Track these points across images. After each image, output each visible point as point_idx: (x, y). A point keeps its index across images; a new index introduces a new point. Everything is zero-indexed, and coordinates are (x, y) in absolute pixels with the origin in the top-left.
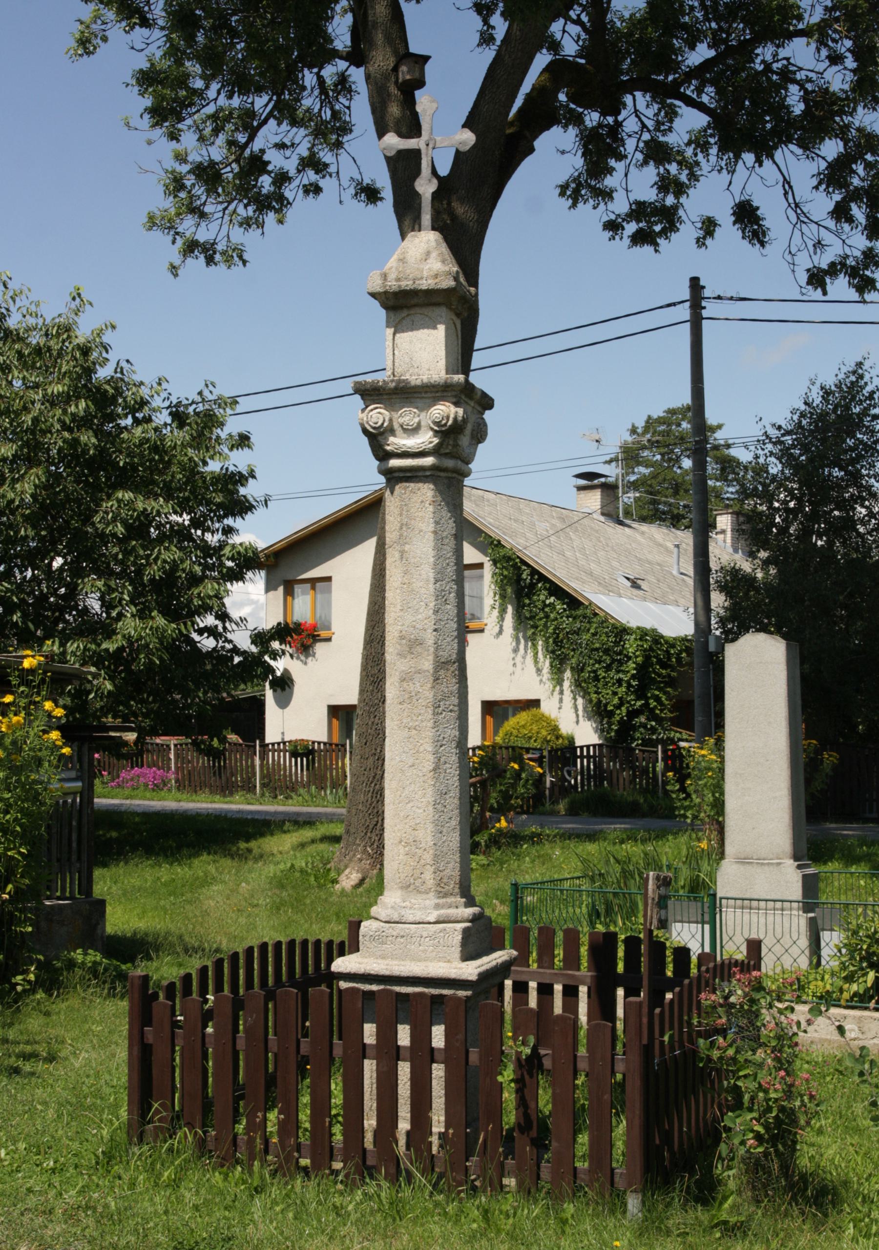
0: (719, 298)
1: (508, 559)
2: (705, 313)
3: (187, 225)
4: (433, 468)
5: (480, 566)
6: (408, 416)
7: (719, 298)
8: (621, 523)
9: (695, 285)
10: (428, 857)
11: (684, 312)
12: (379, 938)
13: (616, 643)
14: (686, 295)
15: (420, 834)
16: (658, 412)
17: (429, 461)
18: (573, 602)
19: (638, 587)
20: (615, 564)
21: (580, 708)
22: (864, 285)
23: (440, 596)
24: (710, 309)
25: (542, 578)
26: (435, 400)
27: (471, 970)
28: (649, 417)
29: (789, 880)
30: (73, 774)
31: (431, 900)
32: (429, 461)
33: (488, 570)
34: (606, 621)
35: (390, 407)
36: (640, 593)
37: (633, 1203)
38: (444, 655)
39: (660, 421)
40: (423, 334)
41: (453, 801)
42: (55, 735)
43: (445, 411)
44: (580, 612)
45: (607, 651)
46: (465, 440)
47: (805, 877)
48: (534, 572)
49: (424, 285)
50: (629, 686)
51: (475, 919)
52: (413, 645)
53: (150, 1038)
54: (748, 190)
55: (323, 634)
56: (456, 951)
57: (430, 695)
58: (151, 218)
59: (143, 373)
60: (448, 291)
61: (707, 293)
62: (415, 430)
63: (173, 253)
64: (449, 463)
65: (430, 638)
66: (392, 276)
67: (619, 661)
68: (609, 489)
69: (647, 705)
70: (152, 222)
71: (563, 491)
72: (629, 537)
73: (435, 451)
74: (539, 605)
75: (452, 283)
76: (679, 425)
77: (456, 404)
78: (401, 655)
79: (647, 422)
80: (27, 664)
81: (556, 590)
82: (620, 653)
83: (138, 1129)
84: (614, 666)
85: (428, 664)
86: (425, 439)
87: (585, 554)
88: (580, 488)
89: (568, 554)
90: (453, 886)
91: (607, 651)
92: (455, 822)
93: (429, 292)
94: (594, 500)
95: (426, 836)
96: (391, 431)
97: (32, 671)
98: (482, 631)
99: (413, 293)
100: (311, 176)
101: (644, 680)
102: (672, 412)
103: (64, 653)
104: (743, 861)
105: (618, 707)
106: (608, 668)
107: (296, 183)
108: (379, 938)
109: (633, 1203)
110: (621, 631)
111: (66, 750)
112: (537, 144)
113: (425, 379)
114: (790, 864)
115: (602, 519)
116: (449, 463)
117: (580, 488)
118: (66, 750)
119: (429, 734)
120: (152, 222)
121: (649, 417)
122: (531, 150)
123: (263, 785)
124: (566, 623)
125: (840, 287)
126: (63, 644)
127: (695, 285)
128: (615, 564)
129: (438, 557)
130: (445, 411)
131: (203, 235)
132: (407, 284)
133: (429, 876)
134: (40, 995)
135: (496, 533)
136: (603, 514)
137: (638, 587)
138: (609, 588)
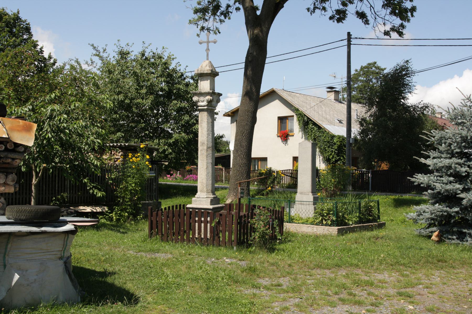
0: (356, 38)
1: (300, 114)
2: (352, 43)
3: (201, 23)
4: (207, 109)
5: (293, 116)
6: (202, 98)
7: (356, 38)
8: (341, 102)
9: (349, 34)
10: (205, 186)
11: (345, 42)
12: (196, 201)
13: (331, 140)
14: (346, 37)
15: (204, 181)
16: (365, 64)
17: (206, 107)
18: (319, 128)
19: (342, 123)
20: (335, 115)
21: (321, 159)
22: (401, 34)
23: (208, 134)
24: (353, 41)
25: (311, 120)
26: (207, 96)
27: (211, 207)
28: (362, 66)
29: (310, 198)
30: (153, 172)
31: (205, 194)
32: (206, 107)
33: (295, 118)
34: (328, 133)
35: (198, 97)
36: (342, 124)
37: (235, 248)
38: (209, 146)
39: (365, 67)
40: (206, 82)
41: (210, 174)
42: (147, 163)
43: (209, 98)
44: (321, 130)
45: (328, 142)
46: (214, 103)
47: (314, 197)
48: (308, 118)
49: (205, 72)
50: (335, 153)
51: (214, 198)
52: (203, 144)
53: (152, 219)
54: (362, 9)
55: (291, 134)
56: (209, 203)
57: (206, 154)
58: (190, 21)
59: (182, 69)
60: (210, 73)
61: (352, 37)
62: (203, 101)
63: (198, 30)
64: (210, 108)
65: (206, 143)
66: (199, 70)
67: (332, 145)
68: (337, 92)
69: (340, 158)
70: (190, 22)
71: (323, 93)
72: (342, 107)
73: (207, 106)
74: (310, 128)
75: (210, 72)
76: (372, 69)
77: (211, 96)
78: (201, 146)
79: (361, 68)
80: (141, 146)
81: (315, 124)
82: (332, 143)
83: (151, 235)
84: (331, 146)
85: (205, 148)
86: (205, 103)
87: (326, 113)
88: (328, 92)
89: (320, 112)
90: (210, 191)
91: (328, 142)
92: (211, 179)
93: (206, 74)
94: (332, 96)
95: (205, 181)
96: (199, 101)
97: (142, 148)
98: (293, 136)
99: (203, 74)
100: (222, 17)
101: (340, 151)
102: (369, 64)
103: (159, 143)
104: (301, 193)
105: (333, 158)
106: (329, 147)
107: (232, 7)
108: (196, 201)
109: (235, 248)
110: (333, 137)
111: (150, 166)
112: (284, 5)
113: (205, 91)
114: (311, 194)
115: (334, 101)
116: (210, 108)
117: (328, 92)
118: (150, 166)
119: (205, 161)
120: (190, 22)
121: (362, 66)
122: (283, 7)
123: (225, 180)
124: (317, 134)
125: (394, 35)
126: (159, 140)
127: (349, 34)
128: (335, 115)
129: (208, 127)
130: (209, 98)
131: (206, 25)
132: (202, 72)
133: (205, 189)
134: (143, 221)
135: (297, 106)
136: (335, 100)
137: (342, 123)
138: (331, 123)
